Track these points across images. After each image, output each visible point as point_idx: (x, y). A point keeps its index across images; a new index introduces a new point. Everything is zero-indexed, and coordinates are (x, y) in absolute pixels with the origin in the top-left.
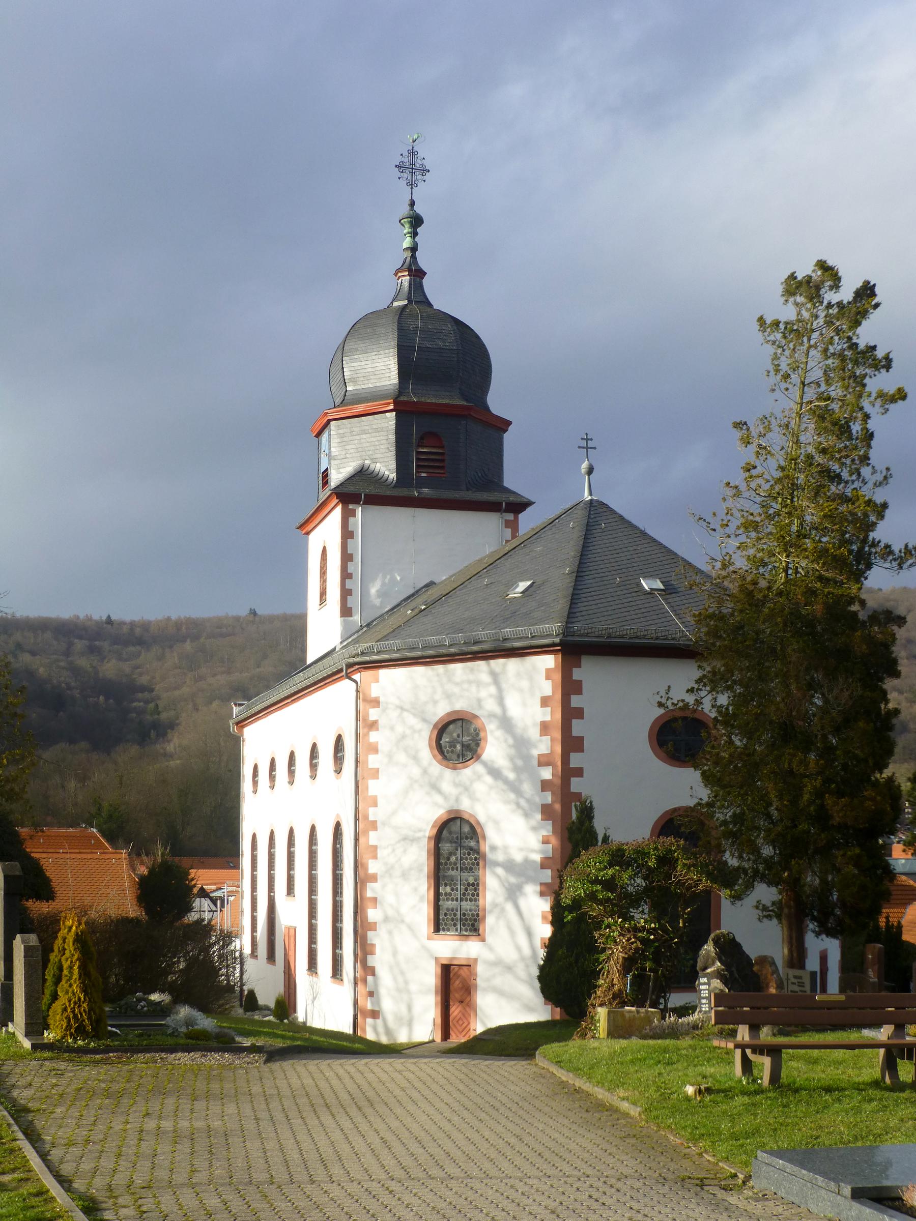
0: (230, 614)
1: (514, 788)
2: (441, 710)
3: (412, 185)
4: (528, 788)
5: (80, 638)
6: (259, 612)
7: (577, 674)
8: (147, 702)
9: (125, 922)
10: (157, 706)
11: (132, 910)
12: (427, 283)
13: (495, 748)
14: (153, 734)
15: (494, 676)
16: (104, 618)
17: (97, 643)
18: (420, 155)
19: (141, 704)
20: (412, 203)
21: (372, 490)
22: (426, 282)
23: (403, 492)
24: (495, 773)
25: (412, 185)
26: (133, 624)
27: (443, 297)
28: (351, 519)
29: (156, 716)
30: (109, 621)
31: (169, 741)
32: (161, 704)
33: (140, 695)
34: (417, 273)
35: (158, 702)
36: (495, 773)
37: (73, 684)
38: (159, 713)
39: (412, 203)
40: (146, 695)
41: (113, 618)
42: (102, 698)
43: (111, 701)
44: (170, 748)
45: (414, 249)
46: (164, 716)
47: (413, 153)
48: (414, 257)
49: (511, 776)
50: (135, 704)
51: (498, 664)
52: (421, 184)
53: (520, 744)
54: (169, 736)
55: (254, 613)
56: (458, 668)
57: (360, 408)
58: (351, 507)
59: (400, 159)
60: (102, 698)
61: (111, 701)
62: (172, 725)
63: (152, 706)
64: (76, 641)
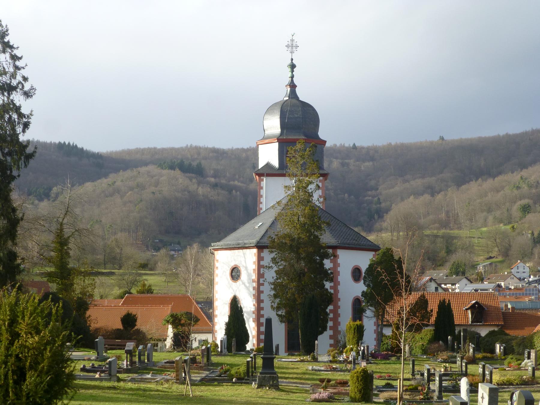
0: (428, 140)
1: (247, 288)
2: (232, 264)
3: (292, 52)
4: (251, 289)
5: (336, 158)
6: (445, 138)
7: (262, 255)
8: (374, 197)
9: (118, 330)
10: (379, 199)
11: (120, 327)
12: (297, 90)
13: (244, 276)
14: (376, 217)
15: (244, 254)
16: (351, 145)
17: (347, 161)
18: (295, 41)
19: (370, 198)
20: (292, 60)
21: (270, 172)
22: (297, 89)
23: (280, 172)
24: (244, 283)
25: (292, 52)
26: (368, 149)
27: (303, 95)
28: (262, 182)
29: (378, 205)
30: (354, 147)
31: (384, 221)
32: (382, 198)
33: (370, 193)
34: (293, 86)
35: (380, 197)
36: (244, 283)
37: (330, 187)
38: (380, 203)
39: (292, 60)
40: (373, 193)
41: (357, 145)
42: (346, 195)
43: (352, 197)
44: (385, 225)
45: (292, 77)
46: (383, 205)
47: (292, 40)
48: (292, 80)
49: (248, 285)
50: (366, 198)
51: (245, 250)
52: (295, 52)
53: (249, 275)
54: (385, 217)
55: (442, 138)
56: (236, 251)
57: (267, 141)
58: (262, 178)
59: (287, 43)
60: (346, 195)
61: (352, 197)
62: (387, 210)
63: (376, 199)
64: (334, 160)
